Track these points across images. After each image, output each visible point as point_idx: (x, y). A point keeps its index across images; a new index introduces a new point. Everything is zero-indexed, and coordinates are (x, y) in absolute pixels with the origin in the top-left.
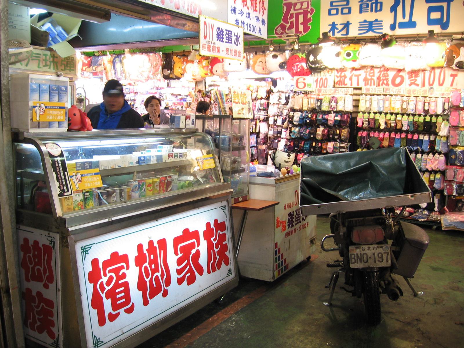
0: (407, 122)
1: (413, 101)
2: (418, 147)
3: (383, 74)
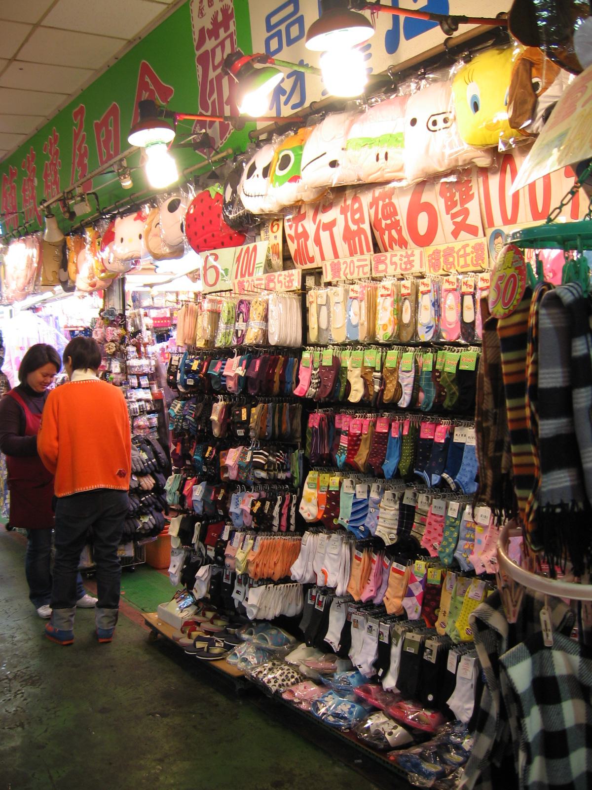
0: (412, 374)
1: (429, 291)
2: (445, 475)
3: (384, 206)
